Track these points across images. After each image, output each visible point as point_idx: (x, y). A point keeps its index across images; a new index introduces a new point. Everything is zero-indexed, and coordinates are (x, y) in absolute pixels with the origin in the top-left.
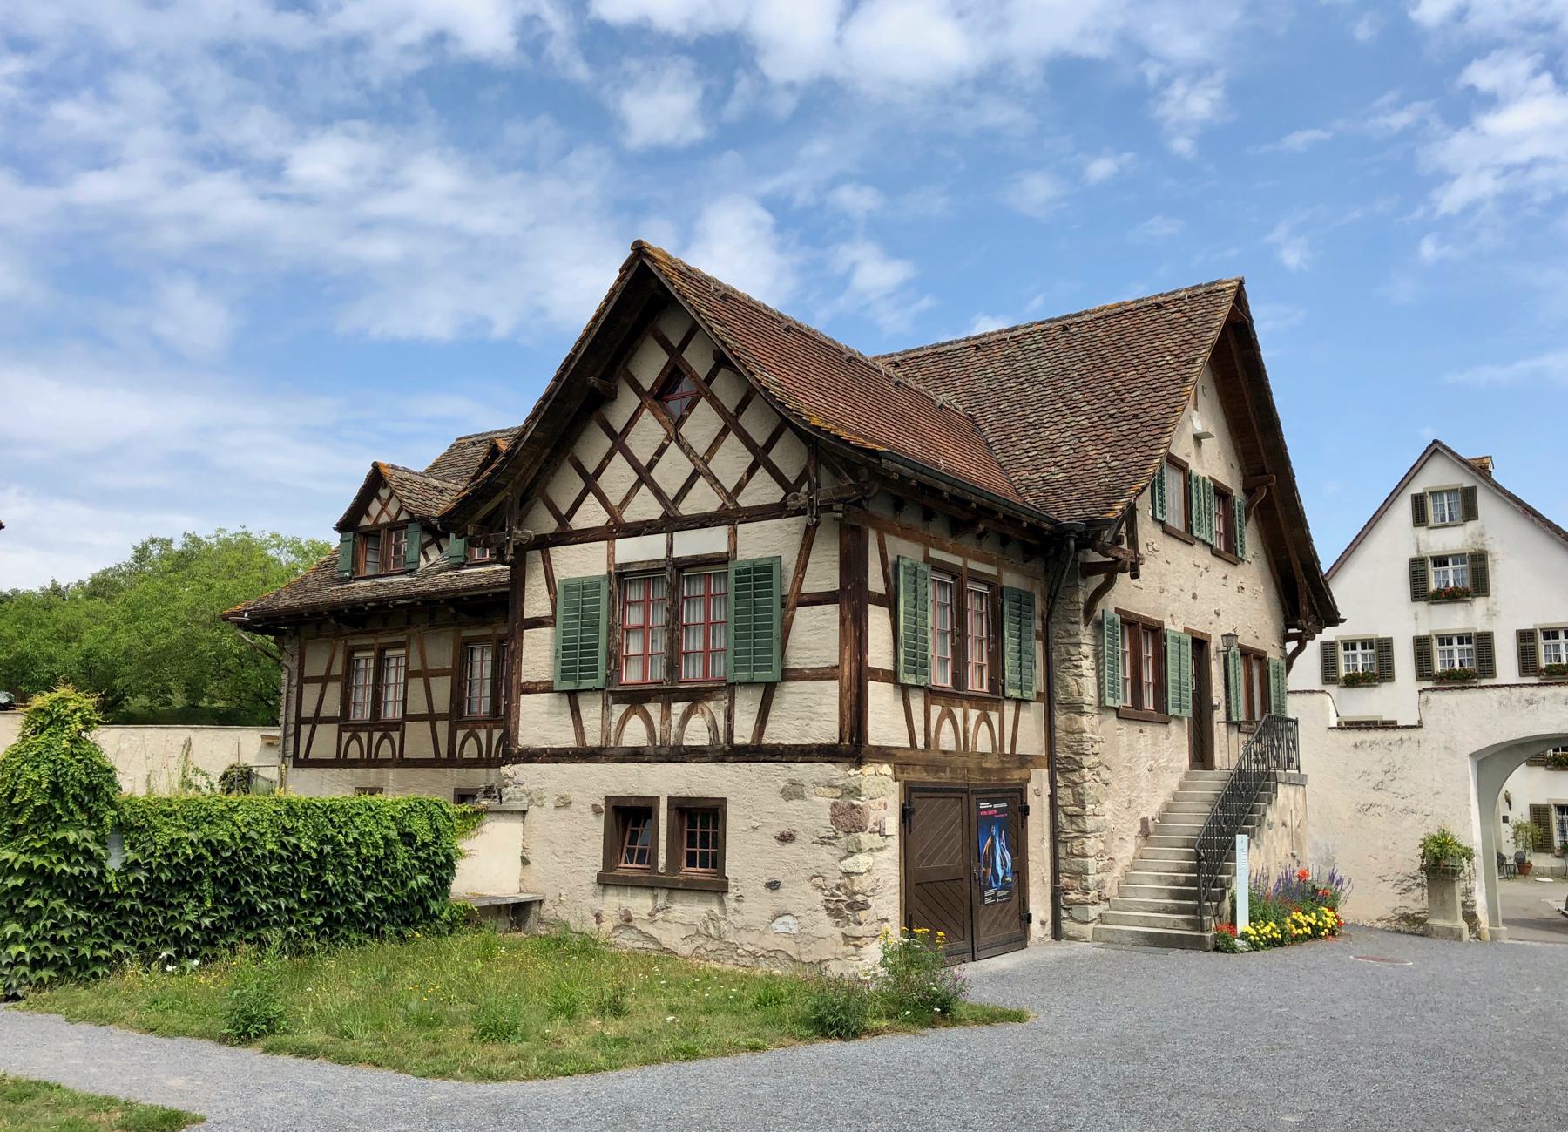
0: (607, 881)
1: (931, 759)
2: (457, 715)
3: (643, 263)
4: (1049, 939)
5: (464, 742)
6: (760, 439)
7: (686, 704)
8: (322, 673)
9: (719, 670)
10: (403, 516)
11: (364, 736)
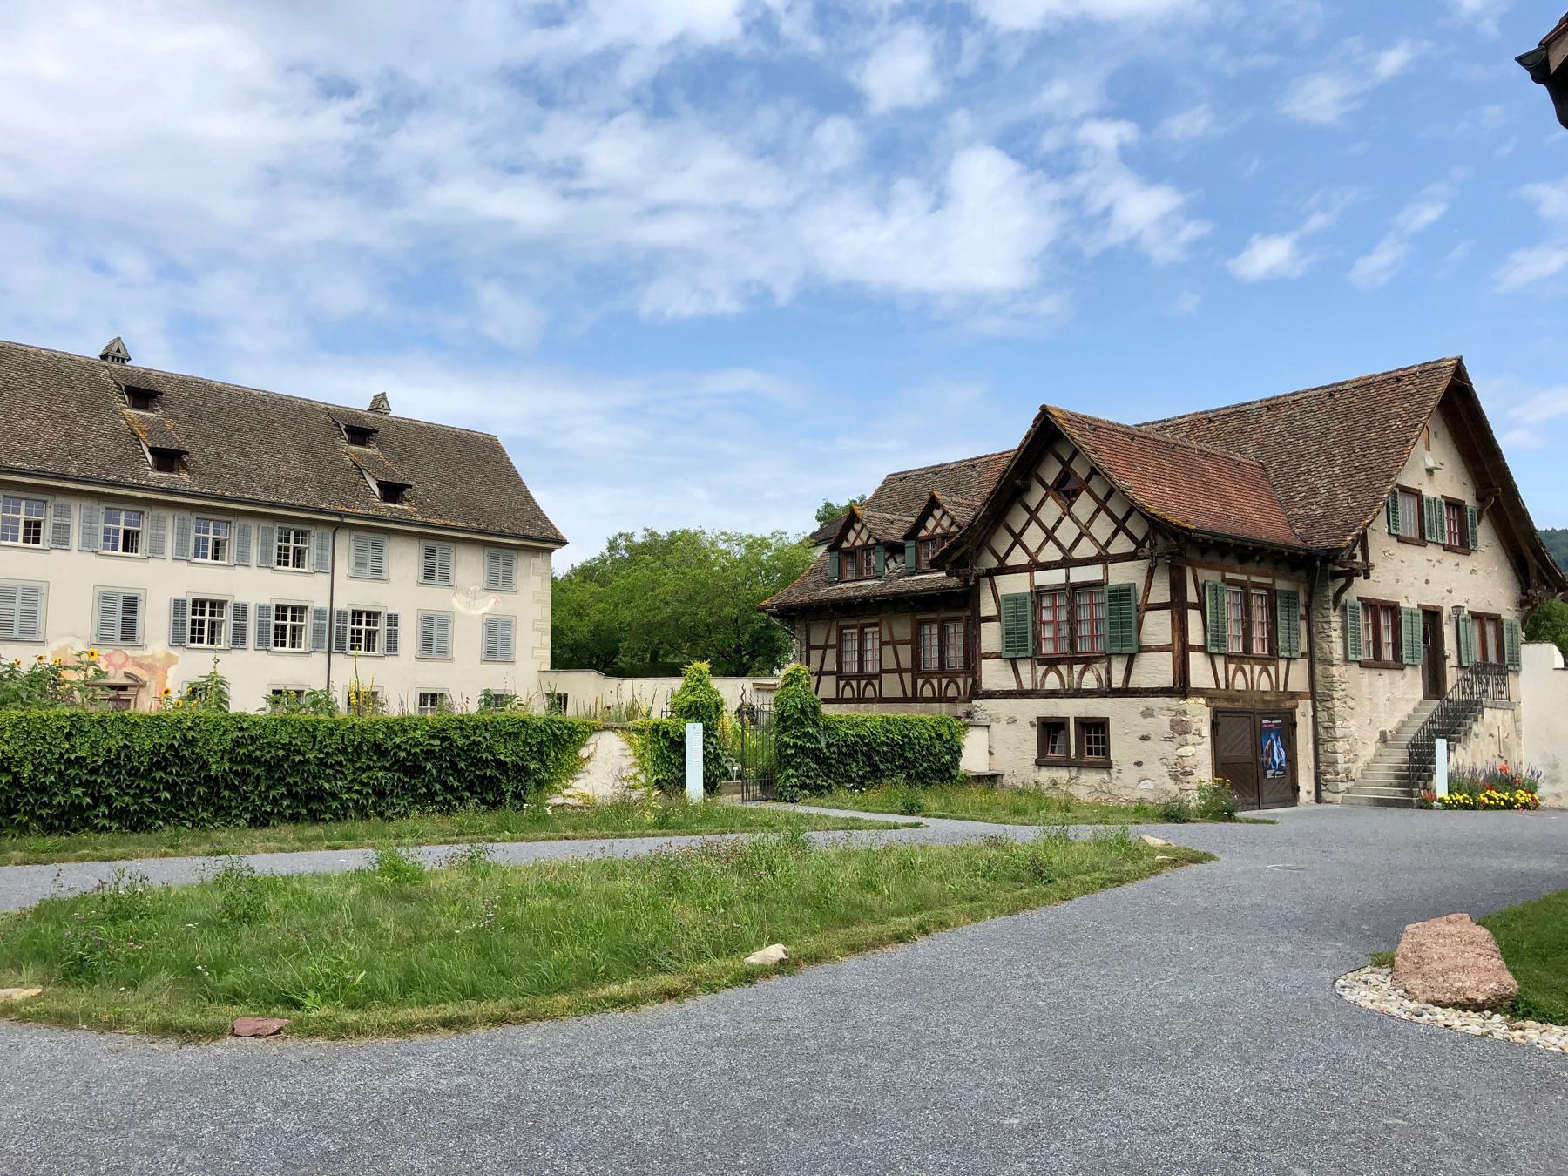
0: (1041, 763)
1: (1229, 694)
2: (917, 669)
3: (1047, 417)
4: (1313, 802)
5: (923, 686)
6: (1120, 516)
7: (1082, 666)
8: (822, 642)
9: (1101, 646)
10: (872, 541)
11: (854, 683)
